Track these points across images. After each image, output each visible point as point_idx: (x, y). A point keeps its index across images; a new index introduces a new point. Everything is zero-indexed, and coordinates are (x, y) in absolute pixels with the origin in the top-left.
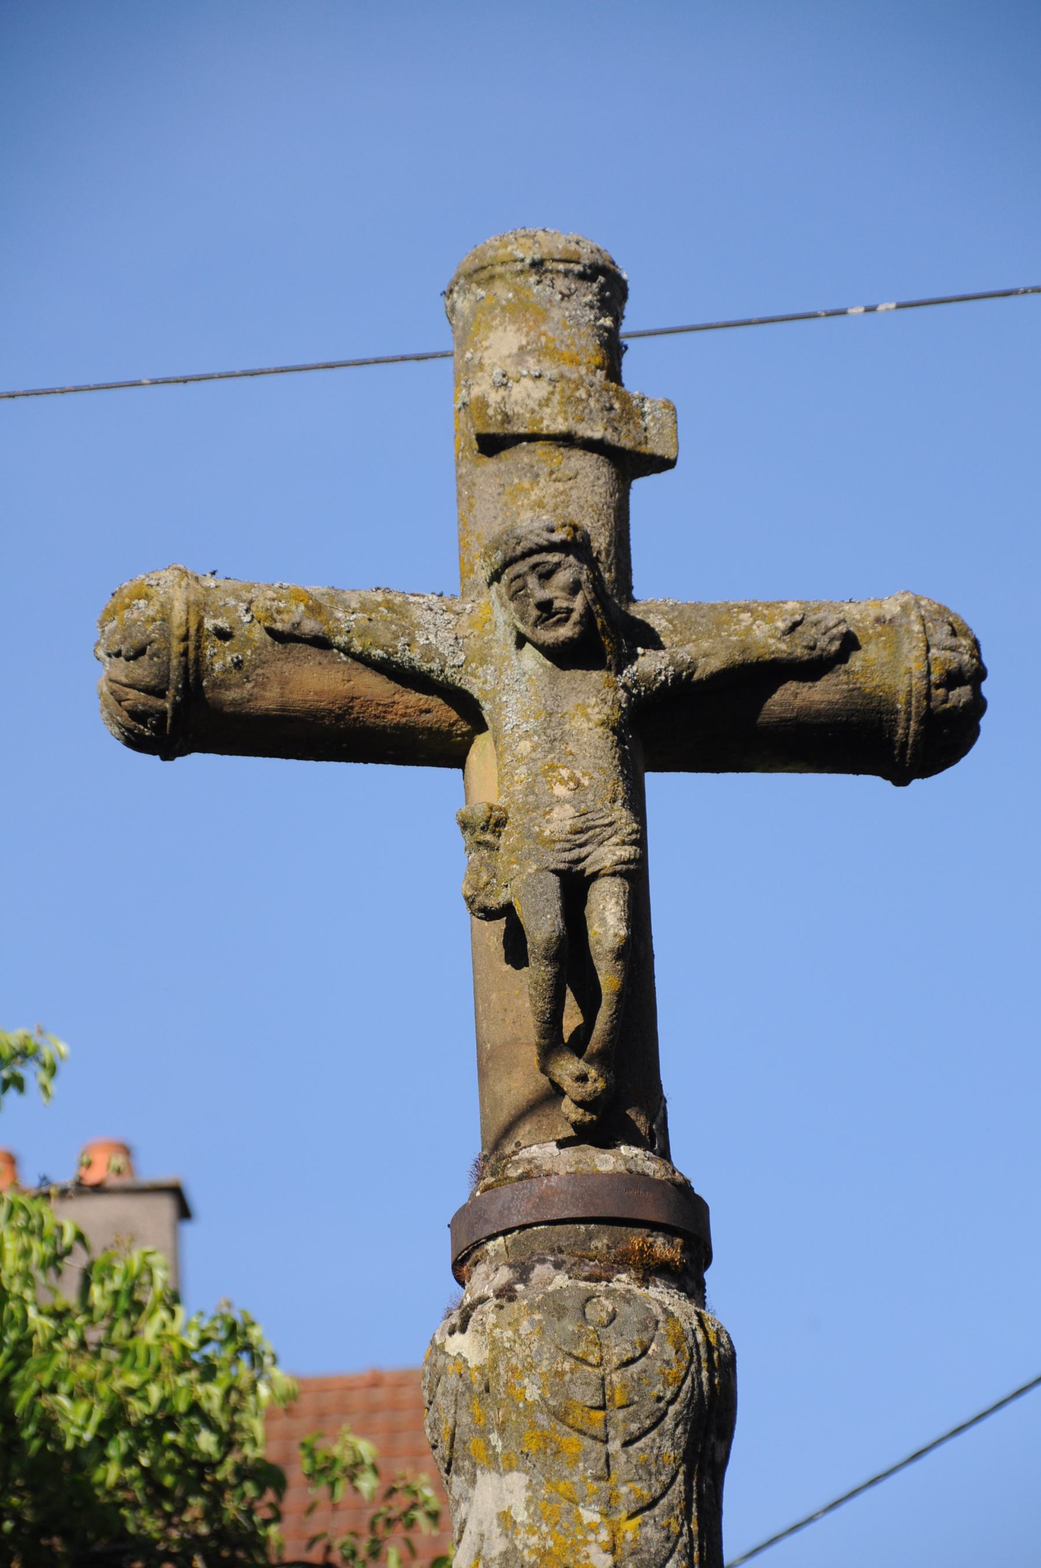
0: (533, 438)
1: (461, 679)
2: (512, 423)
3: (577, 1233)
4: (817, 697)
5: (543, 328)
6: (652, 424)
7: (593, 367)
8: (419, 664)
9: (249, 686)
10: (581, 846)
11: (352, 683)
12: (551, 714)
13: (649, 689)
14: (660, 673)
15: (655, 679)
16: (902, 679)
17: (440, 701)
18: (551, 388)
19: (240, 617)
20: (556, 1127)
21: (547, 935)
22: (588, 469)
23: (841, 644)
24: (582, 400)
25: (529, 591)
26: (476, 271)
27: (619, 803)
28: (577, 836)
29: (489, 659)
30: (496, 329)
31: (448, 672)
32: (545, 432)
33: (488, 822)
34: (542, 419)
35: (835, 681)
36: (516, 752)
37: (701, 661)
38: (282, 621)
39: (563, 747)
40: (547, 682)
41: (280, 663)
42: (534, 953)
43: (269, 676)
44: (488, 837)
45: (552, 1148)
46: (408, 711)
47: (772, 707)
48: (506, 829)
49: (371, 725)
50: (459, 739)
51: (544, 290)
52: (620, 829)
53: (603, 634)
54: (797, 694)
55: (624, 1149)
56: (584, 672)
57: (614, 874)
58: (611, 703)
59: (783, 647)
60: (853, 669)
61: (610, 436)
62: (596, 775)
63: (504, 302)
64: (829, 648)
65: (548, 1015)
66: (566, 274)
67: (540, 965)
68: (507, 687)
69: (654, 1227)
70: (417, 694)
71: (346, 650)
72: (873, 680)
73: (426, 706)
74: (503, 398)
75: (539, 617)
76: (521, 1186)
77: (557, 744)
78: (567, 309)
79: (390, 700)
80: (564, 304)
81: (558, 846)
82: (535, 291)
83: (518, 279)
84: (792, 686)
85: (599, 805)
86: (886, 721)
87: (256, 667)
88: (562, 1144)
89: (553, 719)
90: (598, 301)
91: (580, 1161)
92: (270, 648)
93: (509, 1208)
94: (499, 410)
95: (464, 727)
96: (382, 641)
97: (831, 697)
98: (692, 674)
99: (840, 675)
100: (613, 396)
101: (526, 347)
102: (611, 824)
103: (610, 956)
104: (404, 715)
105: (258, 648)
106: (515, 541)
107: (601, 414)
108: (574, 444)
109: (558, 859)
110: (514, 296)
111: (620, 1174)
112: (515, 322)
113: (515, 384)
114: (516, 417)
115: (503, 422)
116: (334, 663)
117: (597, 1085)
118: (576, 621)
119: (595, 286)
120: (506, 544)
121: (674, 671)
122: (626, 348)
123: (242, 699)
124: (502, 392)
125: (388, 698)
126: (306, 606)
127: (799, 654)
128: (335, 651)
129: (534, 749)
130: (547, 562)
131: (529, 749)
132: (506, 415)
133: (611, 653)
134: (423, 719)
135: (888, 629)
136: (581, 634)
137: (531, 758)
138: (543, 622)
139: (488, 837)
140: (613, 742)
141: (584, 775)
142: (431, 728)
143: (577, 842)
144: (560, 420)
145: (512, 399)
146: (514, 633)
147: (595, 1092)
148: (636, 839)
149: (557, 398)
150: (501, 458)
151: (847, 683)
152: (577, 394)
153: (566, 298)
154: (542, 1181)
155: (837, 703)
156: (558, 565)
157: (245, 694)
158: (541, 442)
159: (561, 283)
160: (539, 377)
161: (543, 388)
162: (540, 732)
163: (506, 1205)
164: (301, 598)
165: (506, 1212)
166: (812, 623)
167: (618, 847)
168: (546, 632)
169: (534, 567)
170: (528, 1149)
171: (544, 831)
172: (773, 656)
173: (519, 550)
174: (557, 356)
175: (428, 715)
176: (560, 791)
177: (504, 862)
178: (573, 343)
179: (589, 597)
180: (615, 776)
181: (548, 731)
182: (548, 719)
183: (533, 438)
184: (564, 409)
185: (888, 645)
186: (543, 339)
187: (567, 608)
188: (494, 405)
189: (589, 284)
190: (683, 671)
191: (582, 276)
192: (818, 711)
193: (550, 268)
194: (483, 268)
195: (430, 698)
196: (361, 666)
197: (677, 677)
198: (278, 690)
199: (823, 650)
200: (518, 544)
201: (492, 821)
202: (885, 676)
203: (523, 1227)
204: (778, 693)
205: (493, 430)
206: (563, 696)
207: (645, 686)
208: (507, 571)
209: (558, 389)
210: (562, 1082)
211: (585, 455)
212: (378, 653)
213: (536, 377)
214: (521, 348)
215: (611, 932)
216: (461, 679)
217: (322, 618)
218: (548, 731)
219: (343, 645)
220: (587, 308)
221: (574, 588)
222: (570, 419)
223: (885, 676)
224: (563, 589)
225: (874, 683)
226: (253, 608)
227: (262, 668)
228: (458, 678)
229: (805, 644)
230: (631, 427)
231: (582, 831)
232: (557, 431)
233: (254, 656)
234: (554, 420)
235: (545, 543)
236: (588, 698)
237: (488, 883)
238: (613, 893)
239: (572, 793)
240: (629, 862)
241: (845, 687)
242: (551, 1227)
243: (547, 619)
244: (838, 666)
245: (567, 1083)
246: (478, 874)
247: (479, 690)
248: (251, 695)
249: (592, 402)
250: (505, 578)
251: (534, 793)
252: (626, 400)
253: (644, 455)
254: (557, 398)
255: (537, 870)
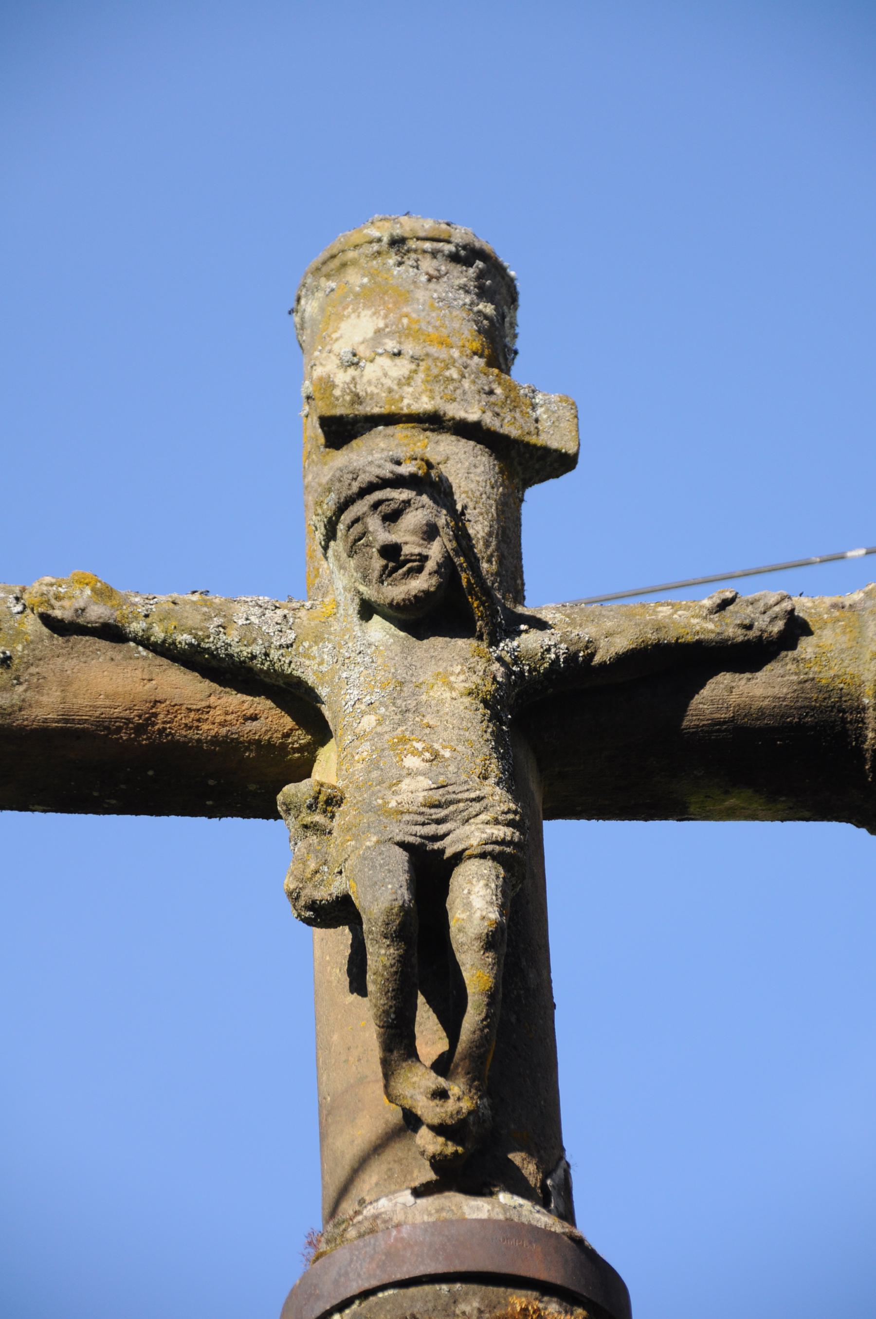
0: (390, 420)
1: (290, 662)
2: (364, 405)
3: (438, 1296)
4: (758, 691)
5: (405, 310)
6: (545, 416)
7: (469, 352)
8: (237, 650)
9: (20, 689)
10: (439, 822)
11: (154, 682)
12: (402, 684)
13: (535, 669)
14: (548, 650)
15: (543, 659)
16: (867, 666)
17: (269, 703)
18: (413, 367)
19: (9, 607)
20: (412, 1173)
21: (387, 905)
22: (462, 456)
23: (786, 624)
24: (453, 380)
25: (371, 538)
26: (324, 263)
27: (492, 780)
28: (433, 811)
29: (326, 636)
30: (349, 316)
31: (274, 654)
32: (406, 411)
33: (316, 798)
34: (402, 398)
35: (781, 671)
36: (357, 731)
37: (602, 643)
38: (63, 607)
39: (417, 719)
40: (399, 651)
41: (60, 660)
42: (371, 932)
43: (46, 675)
44: (318, 818)
45: (407, 1197)
46: (229, 718)
47: (701, 706)
48: (341, 809)
49: (182, 739)
50: (297, 755)
51: (407, 271)
52: (493, 806)
53: (471, 594)
54: (733, 687)
55: (504, 1198)
56: (448, 639)
57: (483, 856)
58: (481, 673)
59: (710, 626)
60: (803, 656)
61: (489, 420)
62: (460, 748)
63: (358, 289)
64: (770, 629)
65: (393, 1016)
66: (434, 254)
67: (380, 947)
68: (347, 661)
69: (545, 1289)
70: (239, 695)
71: (144, 642)
72: (830, 669)
73: (251, 711)
74: (354, 379)
75: (385, 567)
76: (361, 1244)
77: (410, 715)
78: (435, 291)
79: (204, 704)
80: (432, 286)
81: (407, 817)
82: (395, 273)
83: (375, 262)
84: (724, 679)
85: (464, 777)
86: (851, 722)
87: (29, 665)
88: (419, 1192)
89: (405, 689)
90: (475, 287)
91: (442, 1209)
92: (47, 642)
93: (347, 1274)
94: (348, 391)
95: (302, 738)
96: (190, 623)
97: (776, 691)
98: (593, 655)
99: (787, 664)
100: (494, 381)
101: (384, 330)
102: (479, 799)
103: (477, 945)
104: (223, 724)
105: (32, 642)
106: (350, 476)
107: (477, 397)
108: (443, 428)
109: (412, 833)
110: (370, 281)
111: (496, 1222)
112: (369, 307)
113: (368, 364)
114: (369, 397)
115: (353, 403)
116: (131, 658)
117: (462, 1104)
118: (432, 570)
119: (472, 271)
120: (340, 481)
121: (567, 649)
122: (516, 352)
123: (12, 706)
124: (351, 371)
125: (202, 700)
126: (93, 590)
127: (731, 635)
128: (132, 644)
129: (379, 723)
130: (392, 500)
131: (374, 723)
132: (357, 395)
133: (482, 618)
134: (249, 729)
135: (848, 614)
136: (439, 586)
137: (376, 733)
138: (390, 575)
139: (318, 818)
140: (484, 715)
141: (444, 747)
142: (259, 741)
143: (434, 817)
144: (425, 399)
145: (365, 379)
146: (357, 600)
147: (458, 1112)
148: (513, 820)
149: (421, 376)
150: (352, 448)
151: (796, 674)
152: (447, 373)
153: (435, 280)
154: (390, 1234)
155: (785, 699)
156: (407, 503)
157: (16, 699)
158: (401, 425)
159: (428, 265)
160: (399, 354)
161: (403, 366)
162: (388, 702)
163: (343, 1271)
164: (87, 581)
165: (343, 1279)
166: (747, 601)
167: (488, 826)
168: (395, 588)
169: (376, 506)
170: (375, 1204)
171: (388, 803)
172: (697, 637)
173: (355, 487)
174: (422, 338)
175: (254, 723)
176: (412, 762)
177: (338, 845)
178: (443, 325)
179: (449, 546)
180: (486, 750)
181: (399, 702)
182: (398, 688)
183: (390, 420)
184: (429, 387)
185: (848, 630)
186: (405, 321)
187: (420, 554)
188: (341, 385)
189: (464, 268)
190: (579, 651)
191: (454, 258)
192: (761, 709)
193: (414, 246)
194: (333, 257)
195: (257, 699)
196: (165, 661)
197: (572, 657)
198: (58, 693)
199: (763, 631)
200: (355, 479)
201: (322, 798)
202: (845, 664)
203: (365, 1295)
204: (707, 687)
205: (338, 411)
206: (419, 665)
207: (528, 665)
208: (342, 517)
209: (422, 368)
210: (415, 1104)
211: (459, 441)
212: (184, 638)
213: (395, 355)
214: (378, 331)
215: (478, 915)
216: (290, 662)
217: (114, 602)
218: (399, 702)
219: (140, 634)
220: (461, 292)
221: (430, 532)
222: (438, 398)
223: (845, 664)
224: (414, 532)
225: (832, 673)
226: (26, 596)
227: (37, 666)
228: (287, 661)
229: (738, 622)
230: (518, 415)
231: (438, 806)
232: (421, 410)
233: (26, 652)
234: (417, 399)
235: (389, 475)
236: (451, 666)
237: (317, 872)
238: (482, 876)
239: (428, 764)
240: (502, 842)
241: (794, 678)
242: (402, 1291)
243: (395, 570)
244: (783, 653)
245: (420, 1104)
246: (304, 863)
247: (314, 673)
248: (23, 700)
249: (466, 384)
250: (341, 527)
251: (378, 768)
252: (511, 388)
253: (535, 446)
254: (421, 376)
255: (378, 842)
